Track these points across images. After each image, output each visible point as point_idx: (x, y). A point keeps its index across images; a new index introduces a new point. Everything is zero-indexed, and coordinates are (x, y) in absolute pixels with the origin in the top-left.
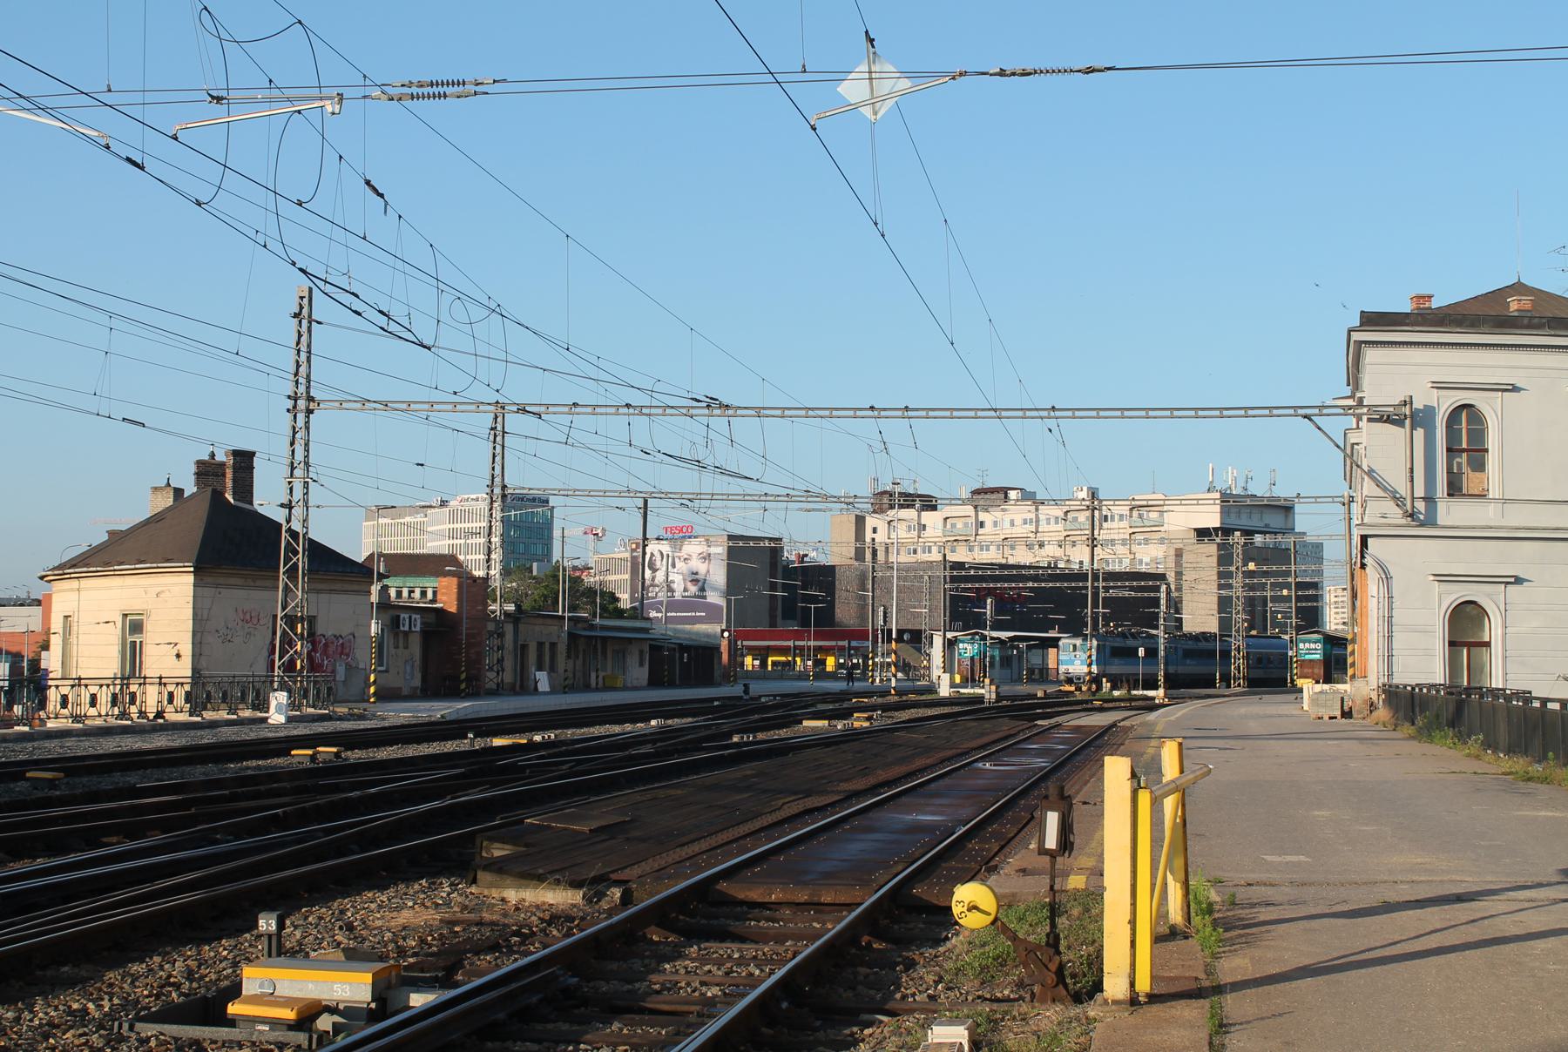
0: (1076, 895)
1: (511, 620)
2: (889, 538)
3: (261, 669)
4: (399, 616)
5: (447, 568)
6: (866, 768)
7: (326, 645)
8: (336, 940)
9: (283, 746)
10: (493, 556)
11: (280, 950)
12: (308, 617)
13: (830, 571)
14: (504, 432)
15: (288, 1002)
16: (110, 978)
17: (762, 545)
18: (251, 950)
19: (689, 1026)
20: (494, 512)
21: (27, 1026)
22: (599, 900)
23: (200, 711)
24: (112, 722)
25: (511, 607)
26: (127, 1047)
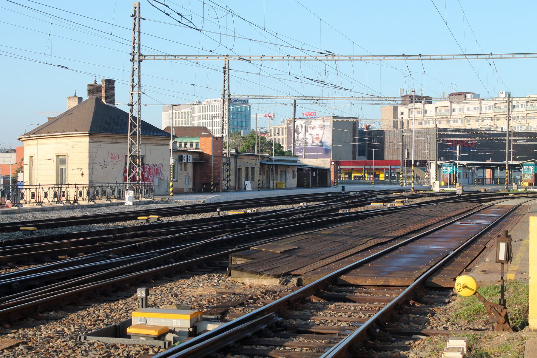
0: (511, 282)
1: (233, 157)
2: (409, 117)
3: (120, 180)
4: (182, 156)
5: (203, 133)
6: (404, 224)
7: (149, 169)
8: (170, 301)
9: (133, 216)
10: (225, 127)
11: (145, 304)
12: (141, 156)
13: (382, 133)
14: (229, 69)
15: (153, 328)
16: (72, 317)
17: (350, 121)
18: (133, 305)
19: (335, 339)
20: (225, 107)
21: (40, 337)
22: (287, 284)
23: (94, 200)
24: (54, 205)
25: (233, 151)
26: (85, 347)
